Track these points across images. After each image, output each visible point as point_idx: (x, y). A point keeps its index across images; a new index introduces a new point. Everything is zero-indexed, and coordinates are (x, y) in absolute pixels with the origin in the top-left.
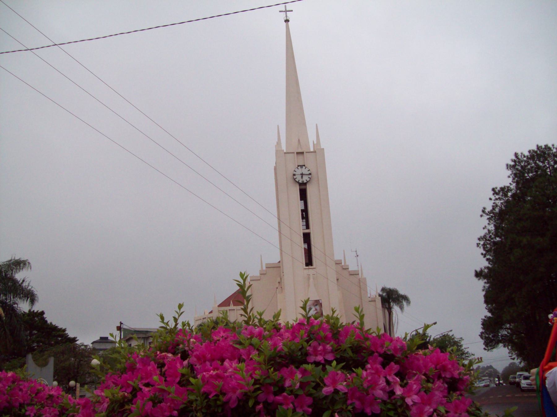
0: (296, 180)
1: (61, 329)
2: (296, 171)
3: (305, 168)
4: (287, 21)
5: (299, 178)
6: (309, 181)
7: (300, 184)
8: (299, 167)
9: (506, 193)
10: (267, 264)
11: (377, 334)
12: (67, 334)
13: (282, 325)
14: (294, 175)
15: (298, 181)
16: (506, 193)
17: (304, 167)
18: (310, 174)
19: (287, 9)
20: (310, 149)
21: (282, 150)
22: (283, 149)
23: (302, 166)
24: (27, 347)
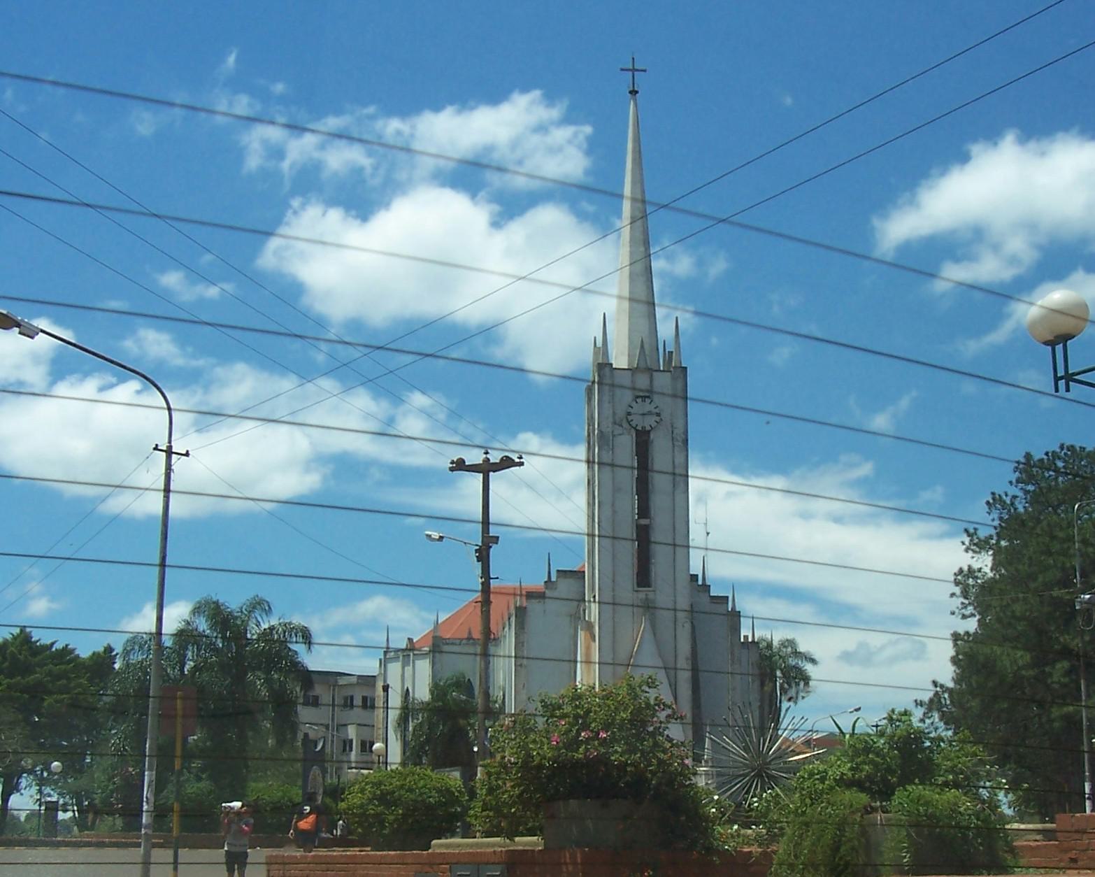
1: (63, 648)
2: (632, 407)
3: (650, 403)
5: (638, 421)
6: (655, 427)
8: (639, 400)
10: (399, 661)
14: (629, 414)
15: (634, 426)
18: (658, 415)
19: (631, 73)
20: (659, 367)
21: (608, 364)
22: (610, 362)
24: (676, 787)
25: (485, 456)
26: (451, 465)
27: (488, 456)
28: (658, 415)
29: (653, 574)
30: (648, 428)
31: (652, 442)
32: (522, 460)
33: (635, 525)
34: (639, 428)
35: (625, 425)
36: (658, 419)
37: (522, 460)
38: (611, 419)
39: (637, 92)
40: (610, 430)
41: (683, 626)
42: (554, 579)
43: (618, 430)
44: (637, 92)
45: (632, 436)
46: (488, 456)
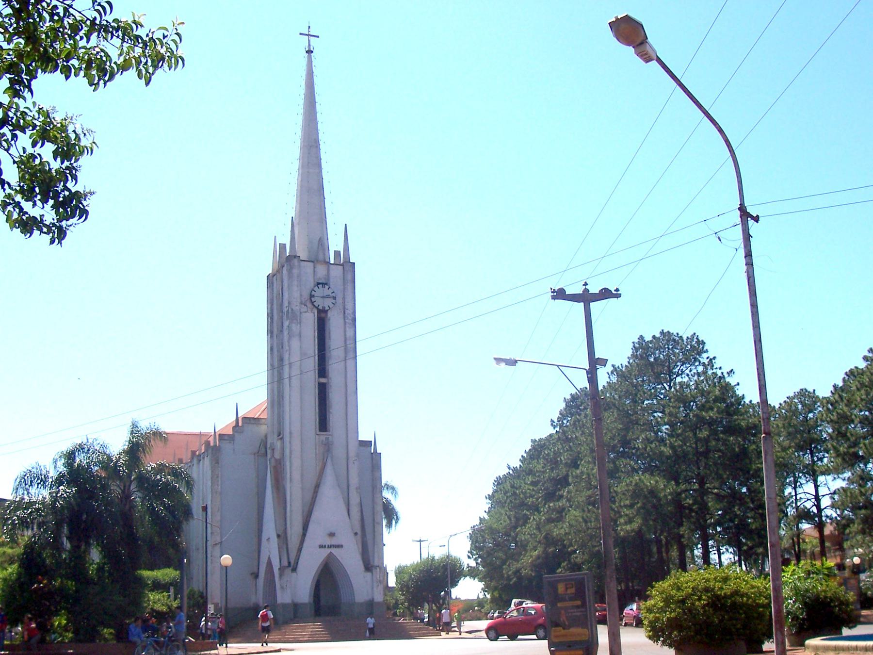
0: (315, 303)
4: (309, 52)
5: (319, 302)
7: (319, 311)
9: (39, 620)
11: (813, 497)
12: (865, 358)
13: (744, 648)
16: (39, 620)
17: (327, 287)
19: (311, 33)
23: (324, 284)
25: (584, 287)
26: (553, 294)
27: (587, 287)
28: (335, 298)
29: (331, 423)
30: (327, 308)
31: (329, 320)
32: (618, 292)
33: (317, 383)
34: (320, 307)
35: (310, 305)
36: (334, 301)
37: (618, 292)
38: (299, 300)
39: (312, 52)
40: (298, 308)
41: (354, 463)
42: (240, 424)
43: (304, 309)
44: (312, 52)
45: (314, 313)
46: (587, 287)
